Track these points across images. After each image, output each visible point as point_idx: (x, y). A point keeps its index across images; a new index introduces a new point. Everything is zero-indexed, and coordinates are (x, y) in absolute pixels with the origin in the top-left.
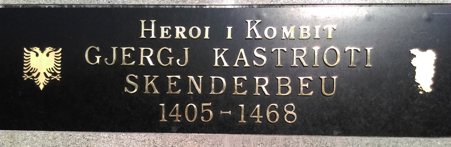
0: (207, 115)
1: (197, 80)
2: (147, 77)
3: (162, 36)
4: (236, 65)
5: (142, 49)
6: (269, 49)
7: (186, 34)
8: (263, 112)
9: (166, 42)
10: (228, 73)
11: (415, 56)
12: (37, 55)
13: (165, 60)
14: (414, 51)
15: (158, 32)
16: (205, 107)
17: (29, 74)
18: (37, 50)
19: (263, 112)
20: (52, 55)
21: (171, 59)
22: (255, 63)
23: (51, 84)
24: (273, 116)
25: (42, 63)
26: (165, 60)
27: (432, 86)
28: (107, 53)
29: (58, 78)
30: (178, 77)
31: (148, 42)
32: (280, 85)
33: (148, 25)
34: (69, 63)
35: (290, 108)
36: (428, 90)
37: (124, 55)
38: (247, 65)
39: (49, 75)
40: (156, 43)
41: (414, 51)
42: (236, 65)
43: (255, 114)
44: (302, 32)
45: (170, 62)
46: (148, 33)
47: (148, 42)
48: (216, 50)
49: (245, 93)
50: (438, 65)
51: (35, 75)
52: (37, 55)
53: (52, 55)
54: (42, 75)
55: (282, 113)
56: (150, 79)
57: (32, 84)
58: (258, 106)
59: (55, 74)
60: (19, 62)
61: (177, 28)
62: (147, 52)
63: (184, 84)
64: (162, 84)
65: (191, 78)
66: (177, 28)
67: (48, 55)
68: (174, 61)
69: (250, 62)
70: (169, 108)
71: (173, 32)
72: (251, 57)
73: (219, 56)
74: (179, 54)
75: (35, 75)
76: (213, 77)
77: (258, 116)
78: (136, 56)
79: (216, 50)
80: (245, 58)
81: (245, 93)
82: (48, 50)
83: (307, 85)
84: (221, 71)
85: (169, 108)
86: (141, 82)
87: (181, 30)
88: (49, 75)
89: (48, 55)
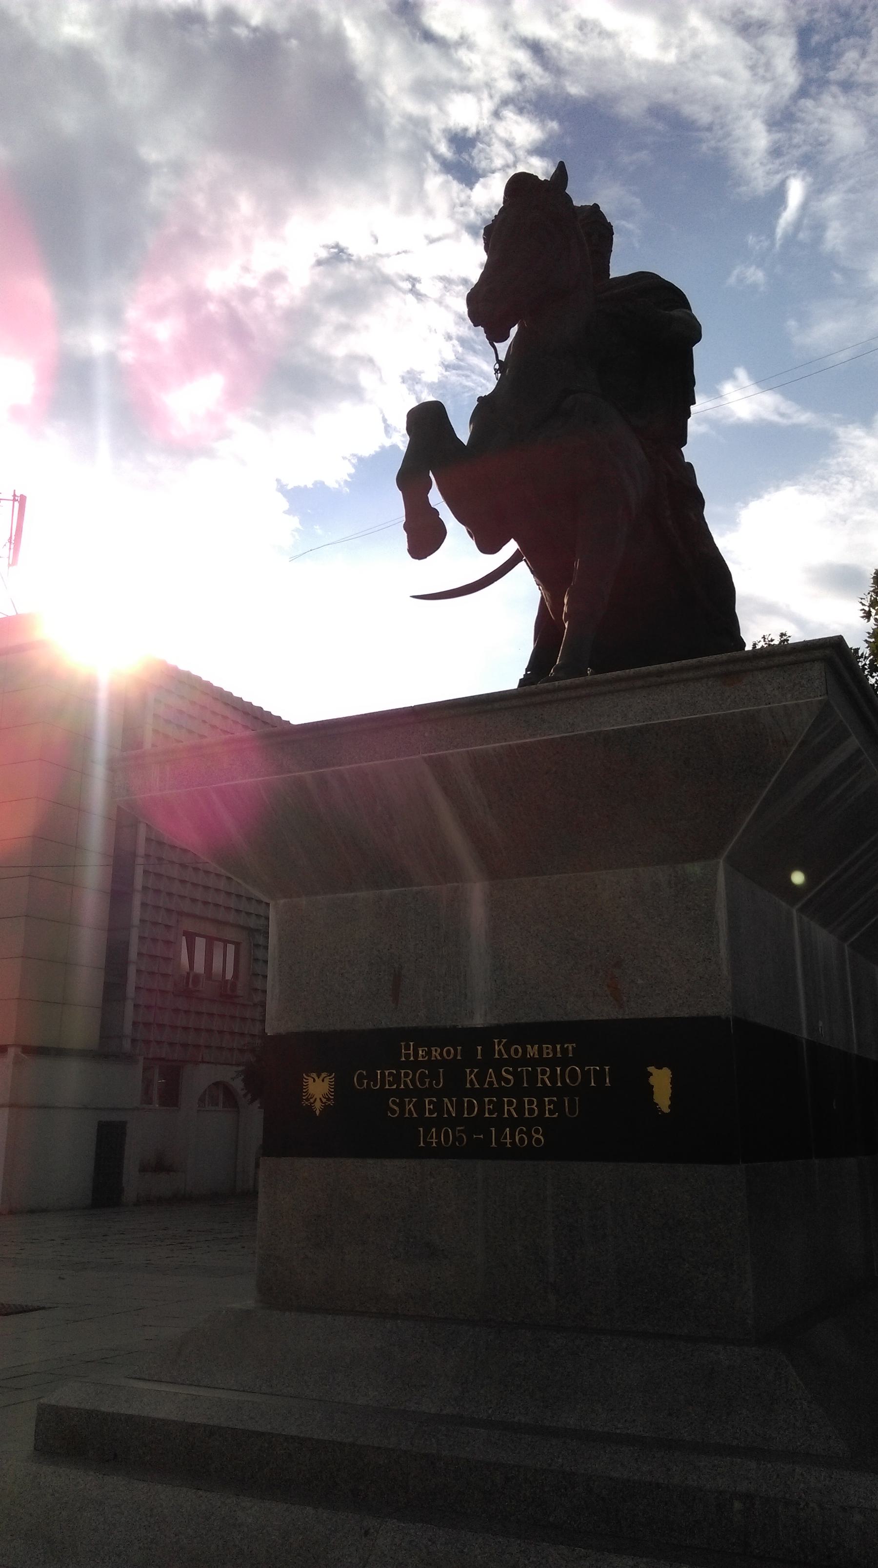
0: (460, 1140)
1: (451, 1102)
2: (407, 1100)
3: (545, 1056)
4: (486, 1086)
5: (403, 1072)
6: (515, 1070)
7: (441, 1054)
8: (512, 1136)
9: (421, 1064)
10: (480, 1094)
11: (651, 1074)
12: (314, 1080)
13: (423, 1083)
14: (651, 1069)
15: (416, 1054)
16: (460, 1131)
17: (308, 1100)
18: (314, 1075)
19: (512, 1136)
20: (327, 1080)
21: (427, 1080)
22: (503, 1084)
23: (326, 1108)
24: (522, 1140)
25: (318, 1088)
26: (423, 1083)
27: (670, 1107)
28: (372, 1077)
29: (331, 1103)
30: (555, 1099)
31: (407, 1064)
32: (527, 1107)
33: (407, 1048)
34: (341, 1088)
35: (537, 1132)
36: (666, 1110)
37: (387, 1079)
38: (496, 1086)
39: (324, 1100)
40: (415, 1065)
41: (651, 1069)
42: (486, 1086)
43: (432, 1138)
44: (545, 1051)
45: (427, 1085)
46: (407, 1056)
47: (407, 1064)
48: (468, 1071)
49: (435, 1115)
50: (673, 1082)
51: (312, 1100)
52: (314, 1080)
53: (327, 1080)
54: (318, 1100)
55: (530, 1137)
56: (410, 1103)
57: (310, 1108)
58: (434, 1130)
59: (329, 1099)
60: (300, 1085)
61: (433, 1049)
62: (544, 1072)
63: (438, 1107)
64: (420, 1107)
65: (446, 1100)
66: (433, 1049)
67: (323, 1081)
68: (430, 1083)
69: (499, 1083)
70: (427, 1132)
71: (429, 1053)
72: (499, 1078)
73: (471, 1076)
74: (434, 1076)
75: (312, 1100)
76: (466, 1100)
77: (434, 1140)
78: (397, 1079)
79: (468, 1071)
80: (494, 1079)
81: (435, 1115)
82: (324, 1075)
83: (552, 1107)
84: (472, 1093)
85: (427, 1132)
86: (402, 1106)
87: (436, 1051)
88: (324, 1100)
89: (323, 1081)
